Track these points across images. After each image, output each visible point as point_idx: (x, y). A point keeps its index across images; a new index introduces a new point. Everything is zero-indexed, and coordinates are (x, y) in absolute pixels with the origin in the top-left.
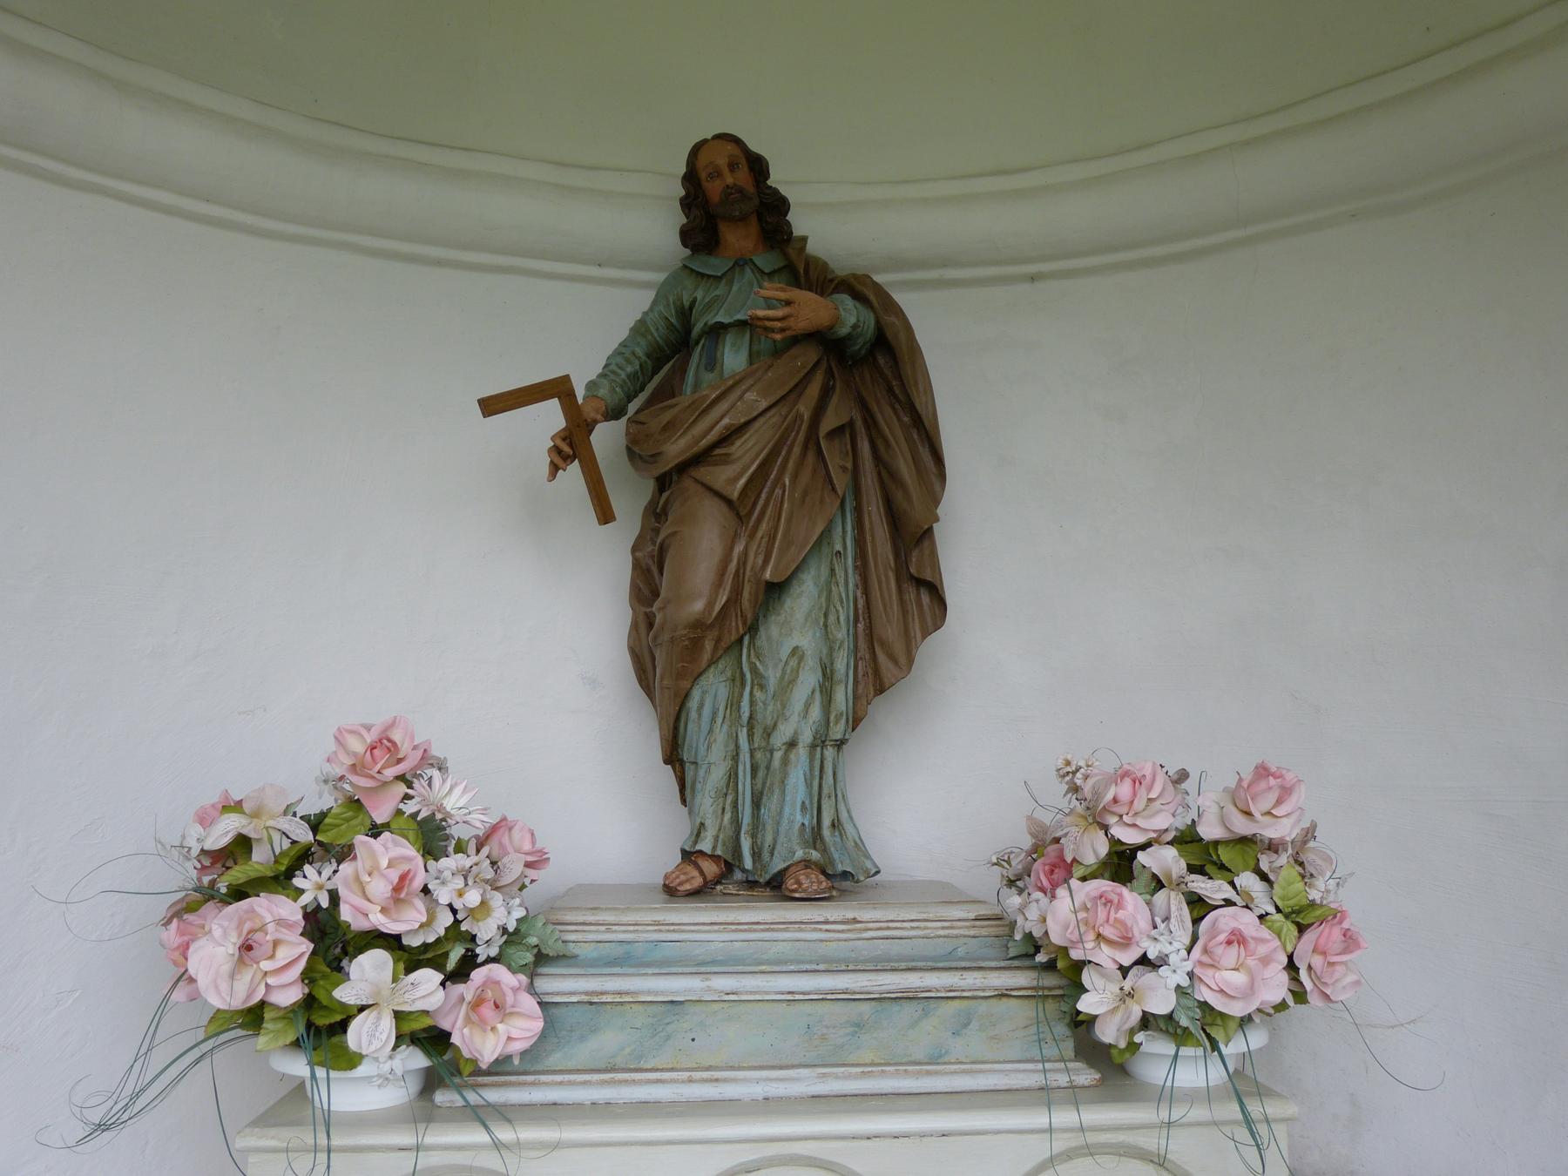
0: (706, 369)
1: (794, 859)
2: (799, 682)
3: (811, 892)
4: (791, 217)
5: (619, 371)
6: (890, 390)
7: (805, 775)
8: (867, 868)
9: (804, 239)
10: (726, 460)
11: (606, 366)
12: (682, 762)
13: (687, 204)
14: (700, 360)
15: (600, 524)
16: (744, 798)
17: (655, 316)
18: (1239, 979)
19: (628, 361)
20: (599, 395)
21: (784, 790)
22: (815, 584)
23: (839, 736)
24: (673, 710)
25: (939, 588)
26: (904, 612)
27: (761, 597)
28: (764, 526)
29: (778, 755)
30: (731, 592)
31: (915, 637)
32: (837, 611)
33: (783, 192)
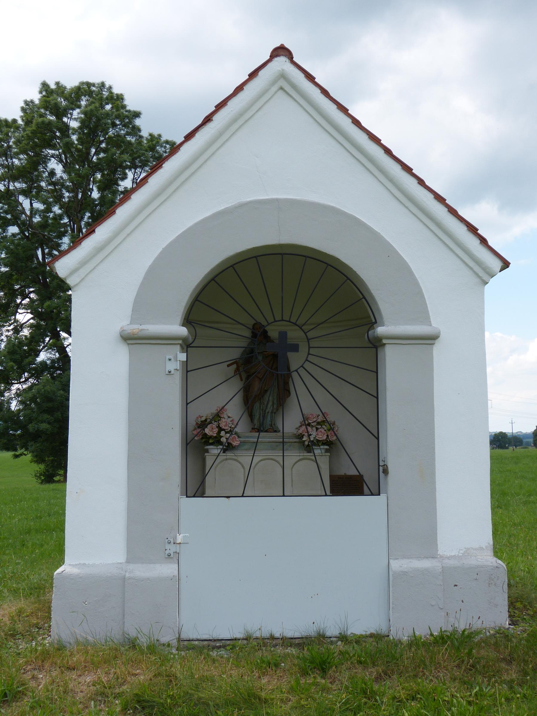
18: (321, 436)
29: (266, 414)
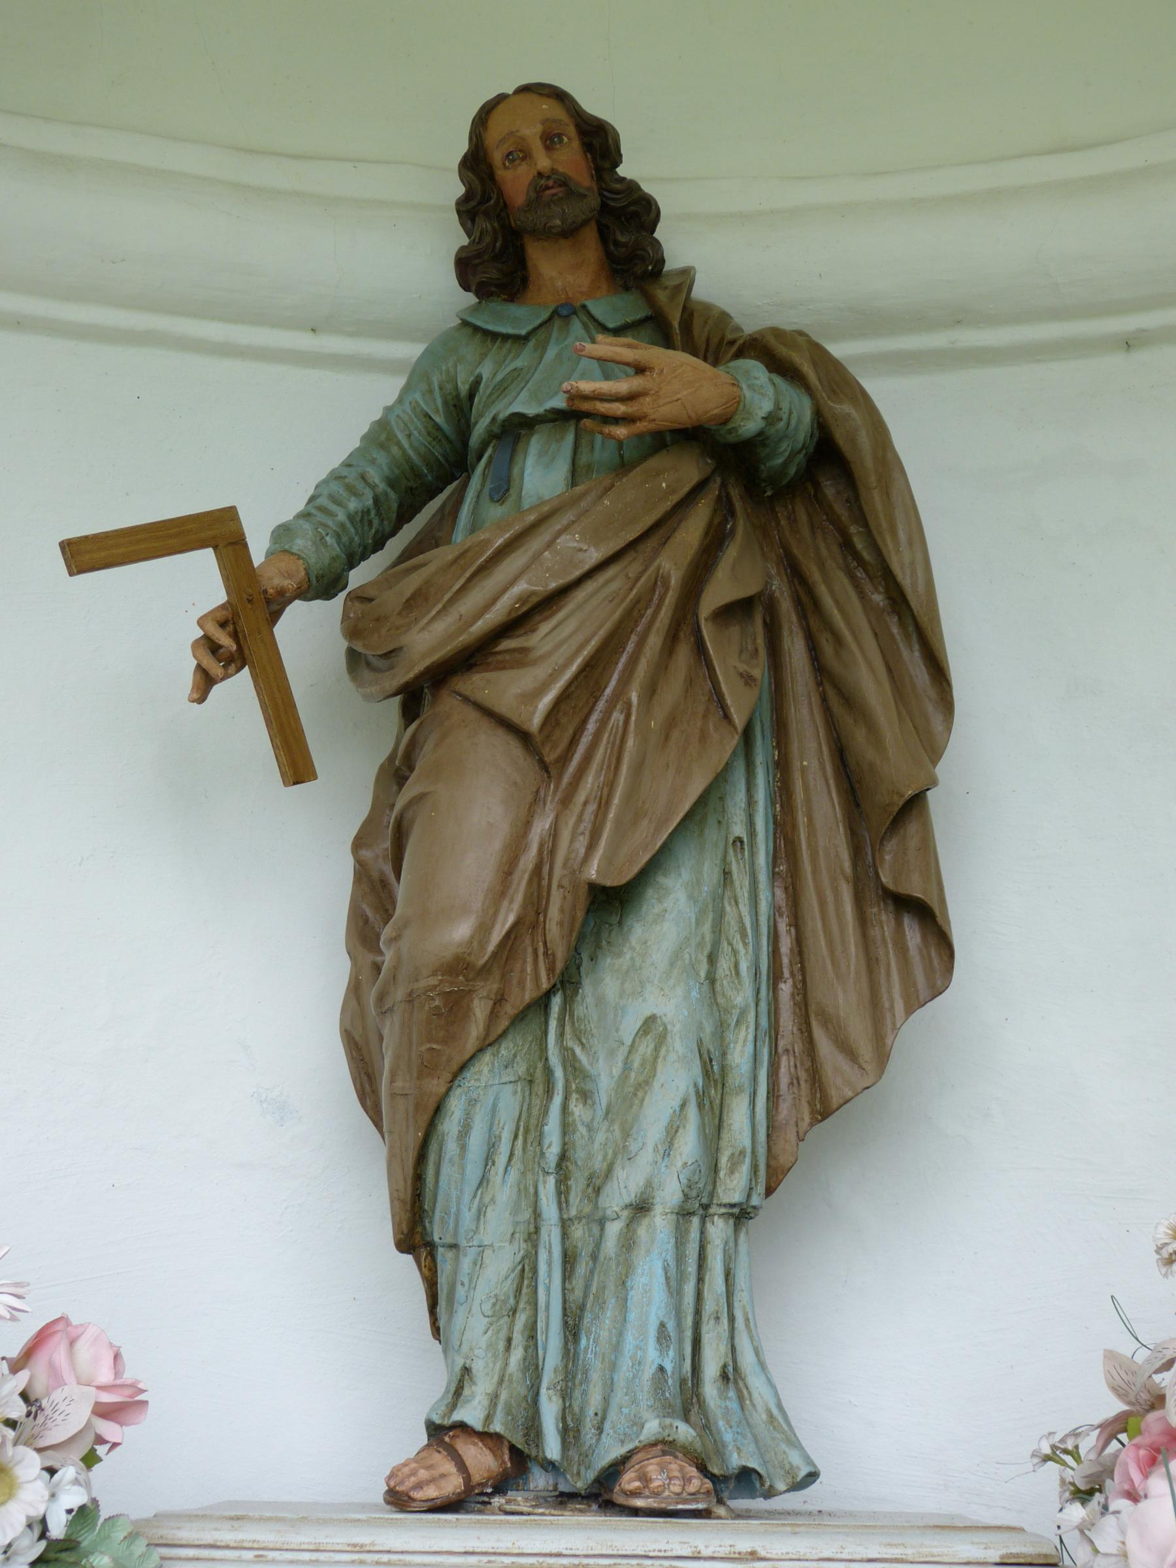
0: (492, 499)
1: (642, 1438)
2: (656, 1084)
3: (668, 1497)
4: (661, 233)
5: (333, 508)
6: (847, 545)
7: (666, 1270)
8: (792, 1467)
9: (687, 274)
10: (522, 658)
11: (312, 499)
12: (431, 1247)
13: (468, 210)
14: (483, 486)
15: (286, 784)
16: (548, 1317)
17: (404, 411)
19: (352, 491)
20: (294, 550)
21: (626, 1300)
22: (691, 897)
23: (737, 1197)
24: (413, 1137)
25: (937, 913)
26: (871, 962)
27: (580, 914)
28: (590, 782)
29: (614, 1229)
30: (524, 906)
31: (892, 1007)
32: (735, 952)
33: (647, 188)
